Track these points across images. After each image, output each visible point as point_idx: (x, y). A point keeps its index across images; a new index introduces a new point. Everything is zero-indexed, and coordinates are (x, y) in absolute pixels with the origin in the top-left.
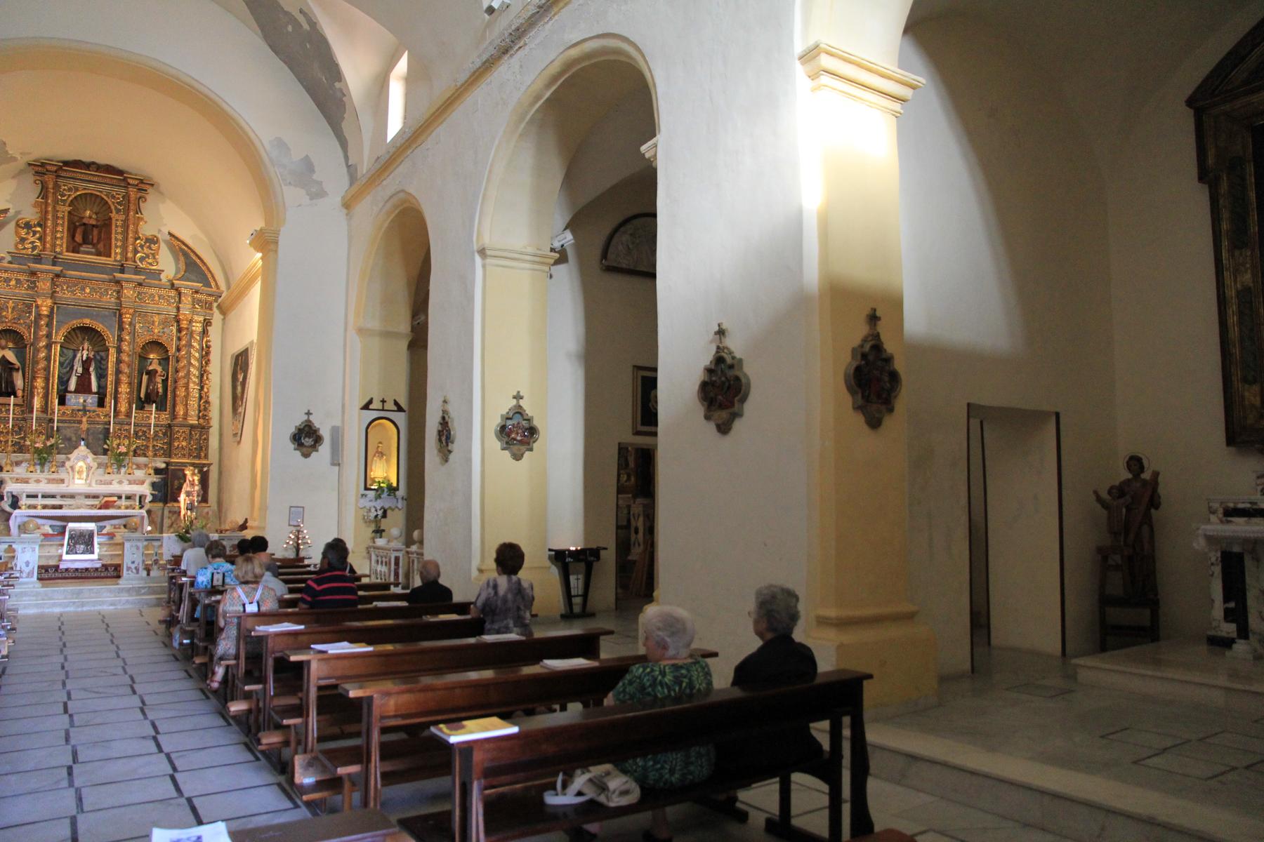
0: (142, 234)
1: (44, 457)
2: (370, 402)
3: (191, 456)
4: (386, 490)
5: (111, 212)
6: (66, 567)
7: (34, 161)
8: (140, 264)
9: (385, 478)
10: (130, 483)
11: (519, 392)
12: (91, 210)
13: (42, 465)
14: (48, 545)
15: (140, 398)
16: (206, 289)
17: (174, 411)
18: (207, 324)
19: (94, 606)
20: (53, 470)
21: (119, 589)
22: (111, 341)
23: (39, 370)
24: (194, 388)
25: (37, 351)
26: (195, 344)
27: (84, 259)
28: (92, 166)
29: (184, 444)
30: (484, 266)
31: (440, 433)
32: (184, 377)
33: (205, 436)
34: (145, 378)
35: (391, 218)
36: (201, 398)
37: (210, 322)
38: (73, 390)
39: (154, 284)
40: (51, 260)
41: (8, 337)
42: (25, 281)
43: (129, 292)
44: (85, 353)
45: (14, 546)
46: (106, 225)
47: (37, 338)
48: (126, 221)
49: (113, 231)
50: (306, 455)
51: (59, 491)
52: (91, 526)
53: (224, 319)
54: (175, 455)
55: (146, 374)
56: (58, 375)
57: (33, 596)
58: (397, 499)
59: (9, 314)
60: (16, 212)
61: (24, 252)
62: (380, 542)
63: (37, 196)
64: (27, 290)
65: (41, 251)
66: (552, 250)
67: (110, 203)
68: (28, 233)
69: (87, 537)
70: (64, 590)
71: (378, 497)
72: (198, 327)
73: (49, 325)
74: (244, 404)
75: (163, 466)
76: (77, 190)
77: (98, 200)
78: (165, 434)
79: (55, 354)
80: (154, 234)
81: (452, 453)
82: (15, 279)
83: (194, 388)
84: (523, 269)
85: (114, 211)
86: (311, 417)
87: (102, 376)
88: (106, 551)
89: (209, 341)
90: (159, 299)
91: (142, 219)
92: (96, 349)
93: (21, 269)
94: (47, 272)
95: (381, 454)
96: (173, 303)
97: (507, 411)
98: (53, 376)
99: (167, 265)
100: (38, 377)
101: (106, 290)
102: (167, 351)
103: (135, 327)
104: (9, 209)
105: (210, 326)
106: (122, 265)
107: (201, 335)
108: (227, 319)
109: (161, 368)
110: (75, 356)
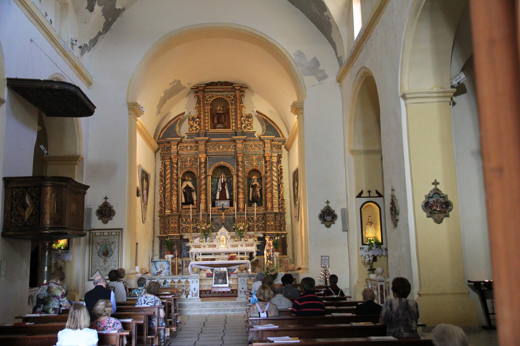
1: (206, 234)
2: (362, 192)
3: (276, 229)
4: (374, 245)
5: (229, 105)
7: (194, 87)
8: (244, 130)
9: (374, 237)
10: (246, 246)
11: (436, 180)
12: (220, 107)
13: (206, 238)
14: (209, 279)
15: (250, 200)
16: (277, 138)
17: (266, 206)
18: (279, 157)
20: (211, 240)
21: (236, 302)
25: (201, 180)
26: (274, 169)
29: (272, 223)
30: (406, 105)
31: (391, 209)
32: (270, 187)
33: (283, 218)
34: (251, 189)
35: (361, 84)
36: (279, 197)
37: (281, 156)
38: (218, 199)
39: (252, 139)
41: (189, 174)
42: (194, 147)
43: (239, 146)
44: (222, 179)
45: (189, 280)
46: (227, 113)
47: (201, 174)
48: (236, 109)
49: (231, 115)
50: (328, 226)
52: (225, 269)
53: (288, 154)
54: (268, 229)
55: (252, 187)
56: (211, 192)
58: (382, 250)
59: (188, 164)
60: (188, 113)
61: (192, 132)
62: (372, 276)
64: (195, 150)
66: (452, 87)
67: (228, 101)
68: (193, 123)
71: (370, 249)
72: (275, 159)
73: (205, 167)
74: (298, 199)
75: (262, 236)
76: (213, 97)
77: (223, 100)
78: (262, 219)
79: (209, 182)
81: (399, 221)
82: (190, 146)
84: (434, 102)
85: (230, 105)
86: (329, 204)
87: (231, 191)
88: (235, 282)
89: (281, 166)
90: (255, 147)
91: (243, 106)
92: (228, 176)
93: (192, 141)
94: (202, 140)
95: (371, 223)
96: (262, 148)
97: (429, 192)
99: (258, 128)
101: (230, 146)
102: (261, 174)
104: (185, 112)
105: (281, 158)
106: (236, 132)
109: (259, 183)
110: (218, 181)
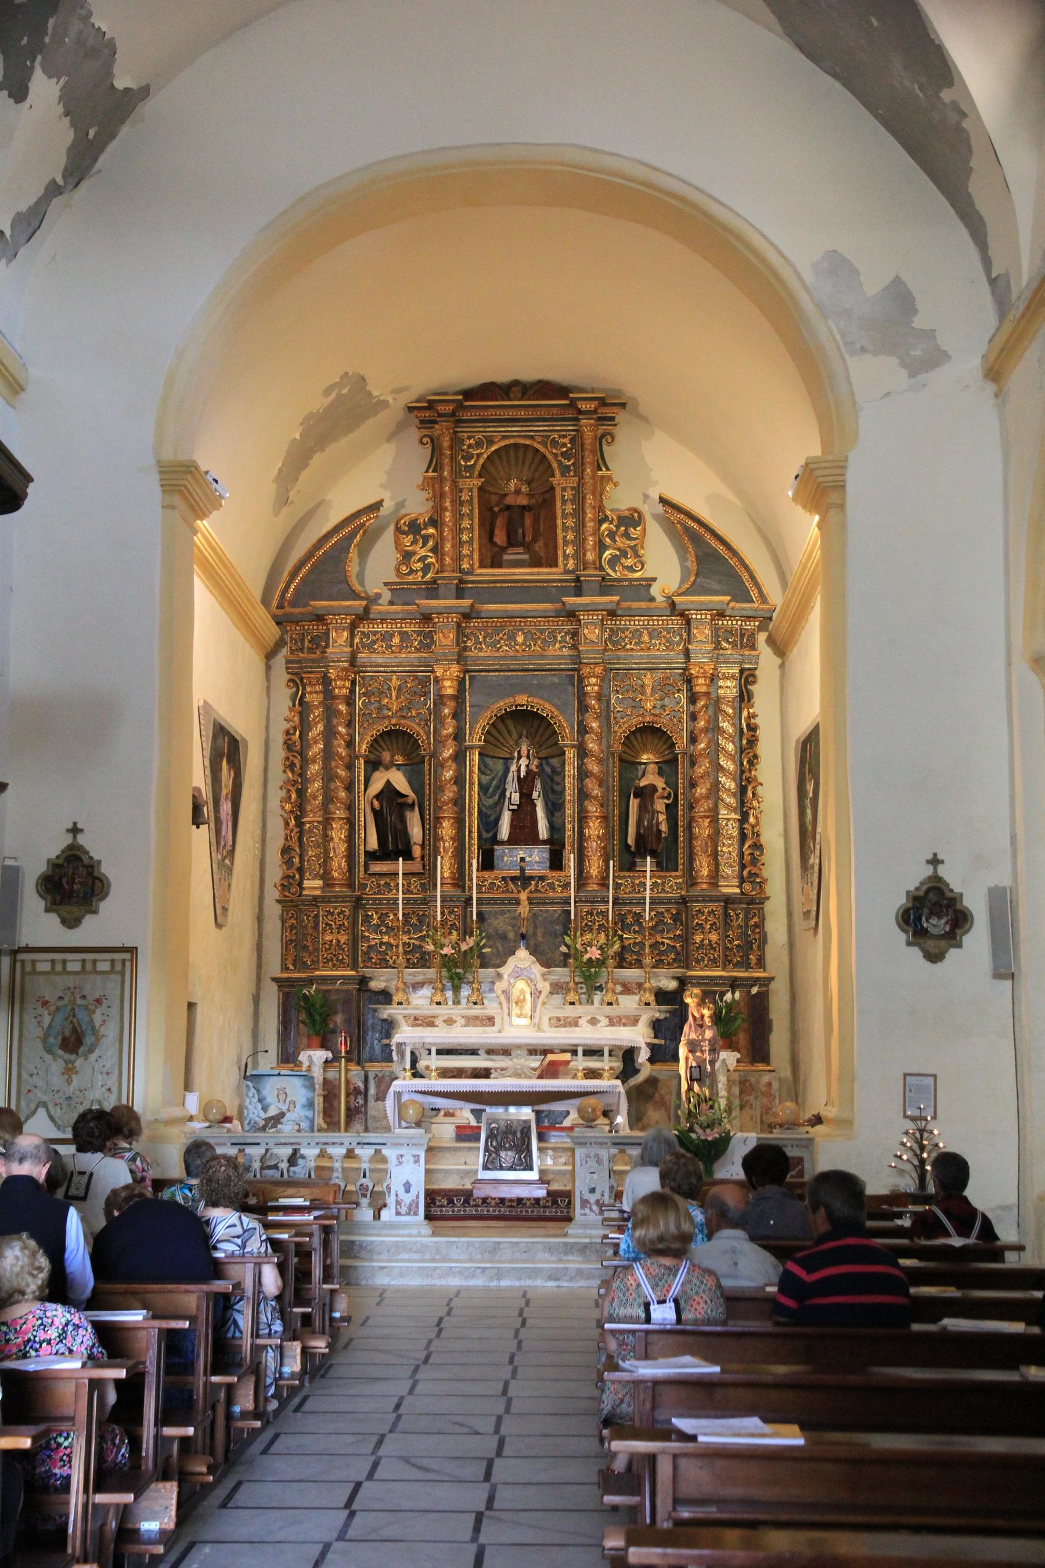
0: (611, 511)
1: (457, 974)
3: (730, 962)
6: (483, 1195)
8: (610, 571)
10: (612, 1023)
15: (628, 846)
16: (739, 605)
18: (746, 679)
19: (520, 1279)
21: (565, 1244)
22: (568, 738)
23: (445, 803)
24: (728, 817)
26: (725, 725)
27: (515, 577)
28: (515, 389)
32: (707, 797)
33: (756, 919)
34: (634, 803)
36: (743, 837)
37: (754, 676)
40: (453, 588)
42: (415, 635)
43: (591, 633)
44: (524, 762)
45: (385, 1151)
49: (559, 513)
50: (934, 957)
51: (483, 1041)
52: (526, 1113)
53: (782, 666)
54: (698, 961)
55: (635, 797)
57: (416, 1252)
61: (411, 578)
63: (425, 469)
64: (418, 650)
65: (437, 573)
67: (549, 456)
68: (414, 542)
69: (519, 1135)
70: (468, 1243)
72: (728, 688)
74: (818, 847)
75: (672, 985)
76: (491, 442)
77: (530, 454)
78: (676, 918)
79: (471, 771)
80: (634, 505)
82: (400, 633)
83: (728, 817)
85: (557, 472)
87: (554, 808)
89: (754, 716)
90: (651, 638)
91: (609, 478)
94: (448, 611)
96: (678, 644)
98: (471, 814)
100: (333, 819)
101: (553, 634)
102: (673, 745)
103: (609, 700)
104: (382, 501)
105: (754, 682)
106: (578, 580)
107: (737, 705)
108: (786, 663)
110: (507, 771)
